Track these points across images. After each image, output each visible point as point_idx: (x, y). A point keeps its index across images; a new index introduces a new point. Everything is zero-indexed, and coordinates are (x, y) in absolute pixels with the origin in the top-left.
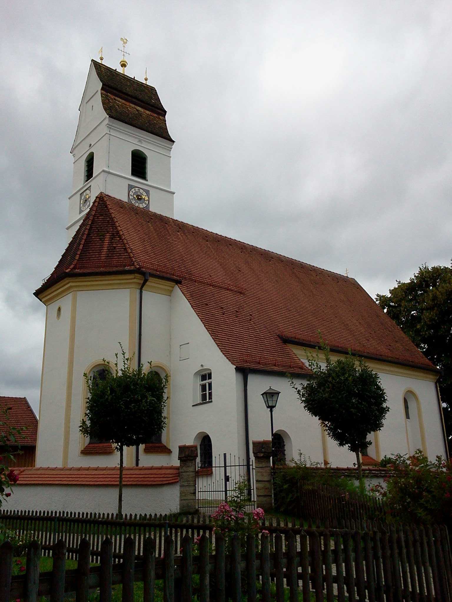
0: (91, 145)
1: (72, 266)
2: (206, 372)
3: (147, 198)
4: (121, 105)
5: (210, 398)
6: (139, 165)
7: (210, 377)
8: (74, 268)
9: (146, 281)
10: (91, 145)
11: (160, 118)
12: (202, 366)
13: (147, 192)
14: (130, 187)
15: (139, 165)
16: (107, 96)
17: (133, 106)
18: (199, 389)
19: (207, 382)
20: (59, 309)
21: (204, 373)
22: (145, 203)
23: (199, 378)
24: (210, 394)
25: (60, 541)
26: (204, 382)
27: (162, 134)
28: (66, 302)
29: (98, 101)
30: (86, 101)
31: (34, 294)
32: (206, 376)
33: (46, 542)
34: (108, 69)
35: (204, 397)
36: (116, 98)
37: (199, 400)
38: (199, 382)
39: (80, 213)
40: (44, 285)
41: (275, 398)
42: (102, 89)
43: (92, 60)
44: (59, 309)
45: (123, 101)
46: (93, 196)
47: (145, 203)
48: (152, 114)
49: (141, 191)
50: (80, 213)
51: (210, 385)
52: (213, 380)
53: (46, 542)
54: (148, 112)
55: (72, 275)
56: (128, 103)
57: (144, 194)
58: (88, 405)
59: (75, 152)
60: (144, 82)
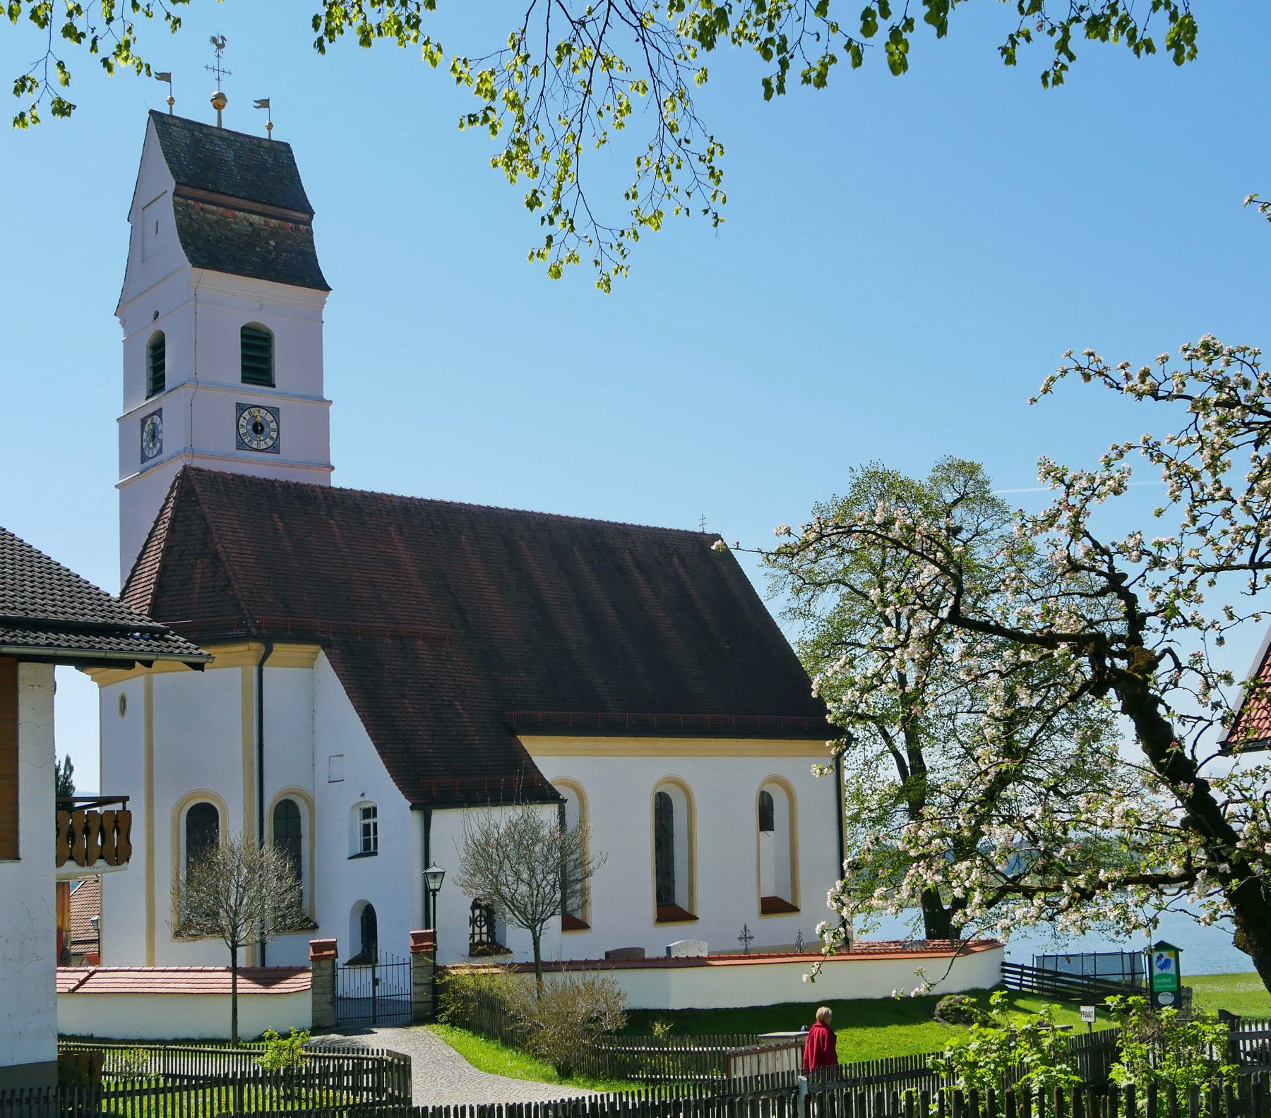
0: (157, 314)
2: (370, 805)
3: (273, 426)
4: (217, 222)
5: (376, 847)
6: (257, 355)
7: (375, 815)
9: (268, 652)
10: (157, 314)
13: (274, 412)
14: (241, 408)
15: (257, 355)
17: (241, 214)
19: (371, 821)
20: (123, 700)
21: (366, 806)
22: (271, 438)
23: (359, 814)
24: (376, 840)
25: (355, 1095)
26: (367, 821)
27: (303, 271)
32: (369, 812)
33: (660, 1090)
35: (366, 844)
37: (359, 848)
38: (360, 822)
39: (142, 462)
43: (152, 112)
44: (123, 700)
45: (222, 209)
46: (168, 473)
47: (271, 438)
50: (142, 462)
51: (375, 825)
52: (378, 820)
53: (660, 1090)
54: (274, 222)
56: (230, 212)
57: (269, 417)
60: (263, 134)
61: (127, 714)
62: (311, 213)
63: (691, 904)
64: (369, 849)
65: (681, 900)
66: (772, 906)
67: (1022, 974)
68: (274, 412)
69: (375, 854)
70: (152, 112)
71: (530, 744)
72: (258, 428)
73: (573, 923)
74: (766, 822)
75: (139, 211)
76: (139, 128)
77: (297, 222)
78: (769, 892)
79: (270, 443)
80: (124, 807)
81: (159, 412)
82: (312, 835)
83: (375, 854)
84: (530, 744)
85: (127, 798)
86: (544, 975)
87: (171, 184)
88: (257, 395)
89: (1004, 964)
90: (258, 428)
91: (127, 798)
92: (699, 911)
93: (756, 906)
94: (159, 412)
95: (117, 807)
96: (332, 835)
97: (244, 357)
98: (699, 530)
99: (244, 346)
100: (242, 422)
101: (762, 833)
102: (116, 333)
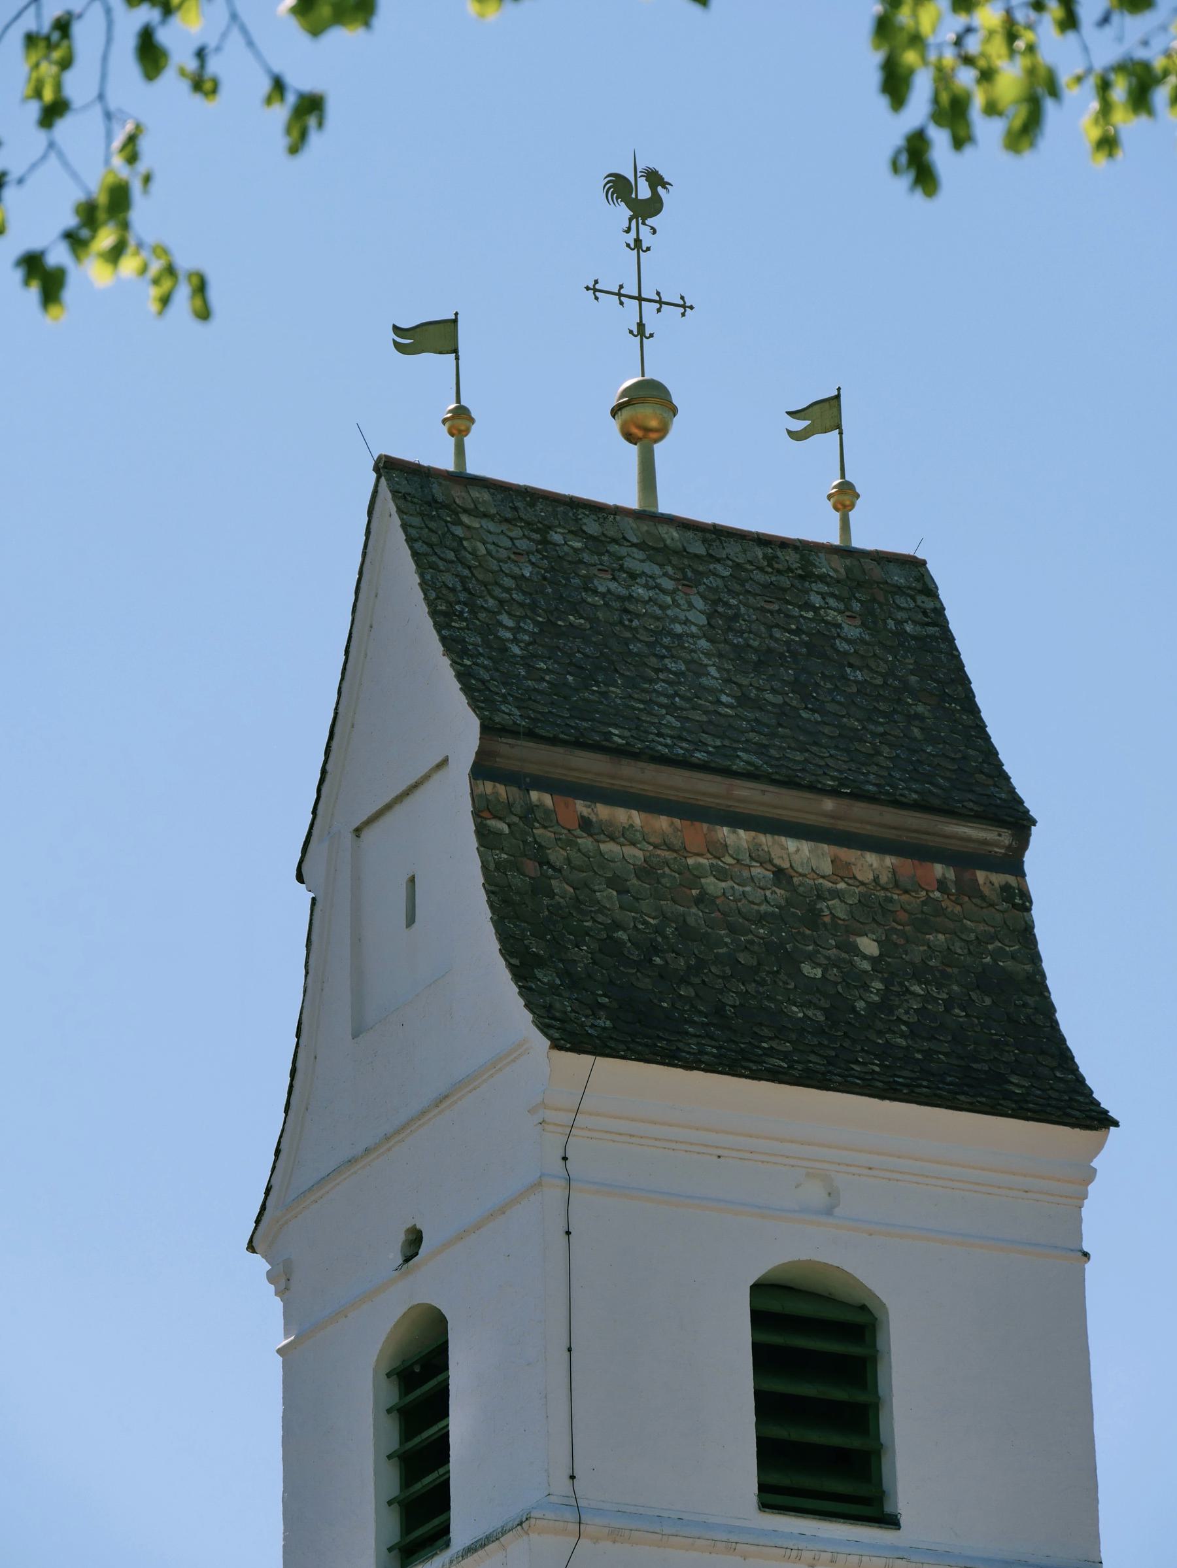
0: (414, 1241)
4: (647, 871)
10: (414, 1241)
11: (974, 891)
17: (743, 838)
36: (603, 812)
42: (481, 770)
45: (663, 823)
48: (907, 867)
54: (871, 865)
56: (694, 834)
62: (1019, 822)
75: (336, 842)
77: (965, 860)
99: (765, 1359)
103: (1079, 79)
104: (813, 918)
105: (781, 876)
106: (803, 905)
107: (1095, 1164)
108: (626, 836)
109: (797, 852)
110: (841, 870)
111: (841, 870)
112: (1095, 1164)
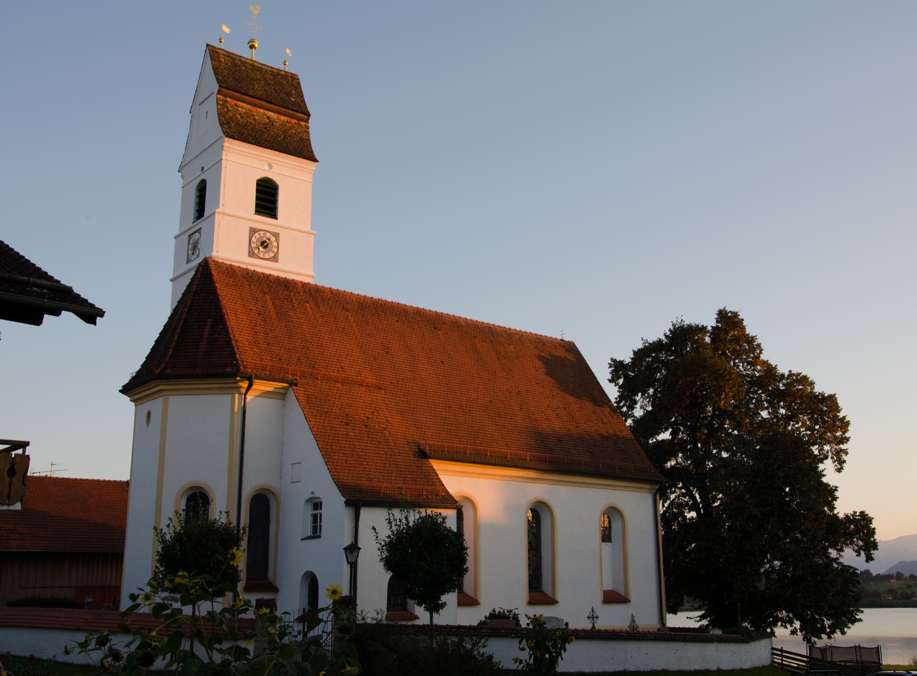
0: (203, 168)
1: (163, 365)
3: (275, 244)
4: (245, 113)
8: (166, 368)
10: (203, 168)
11: (300, 125)
12: (313, 493)
13: (276, 235)
16: (226, 101)
17: (262, 111)
18: (310, 519)
20: (149, 414)
23: (310, 507)
26: (316, 512)
28: (155, 405)
29: (212, 107)
30: (197, 104)
31: (120, 391)
32: (317, 505)
34: (230, 56)
36: (239, 103)
37: (309, 533)
38: (310, 511)
39: (188, 263)
40: (133, 379)
41: (355, 554)
42: (219, 92)
44: (149, 414)
45: (249, 106)
48: (289, 120)
49: (268, 235)
50: (188, 263)
54: (283, 118)
55: (164, 377)
56: (254, 109)
57: (273, 239)
58: (157, 558)
59: (183, 172)
61: (151, 425)
62: (308, 115)
63: (554, 592)
64: (316, 533)
65: (546, 588)
66: (613, 598)
67: (783, 656)
68: (276, 235)
69: (320, 537)
70: (208, 45)
71: (437, 465)
72: (264, 244)
73: (468, 601)
74: (606, 536)
75: (198, 102)
76: (200, 53)
77: (300, 119)
78: (608, 587)
79: (272, 255)
80: (24, 452)
81: (199, 231)
82: (278, 521)
83: (320, 537)
84: (437, 465)
85: (27, 444)
86: (191, 614)
87: (216, 87)
88: (264, 222)
89: (773, 649)
90: (264, 244)
91: (27, 444)
92: (559, 597)
93: (600, 597)
94: (199, 231)
95: (20, 451)
96: (292, 520)
97: (257, 198)
98: (559, 337)
99: (258, 191)
100: (254, 239)
101: (604, 544)
102: (178, 181)
103: (270, 166)
104: (273, 125)
105: (268, 118)
106: (271, 122)
107: (63, 312)
108: (242, 108)
109: (271, 114)
110: (278, 118)
111: (278, 118)
112: (63, 312)
